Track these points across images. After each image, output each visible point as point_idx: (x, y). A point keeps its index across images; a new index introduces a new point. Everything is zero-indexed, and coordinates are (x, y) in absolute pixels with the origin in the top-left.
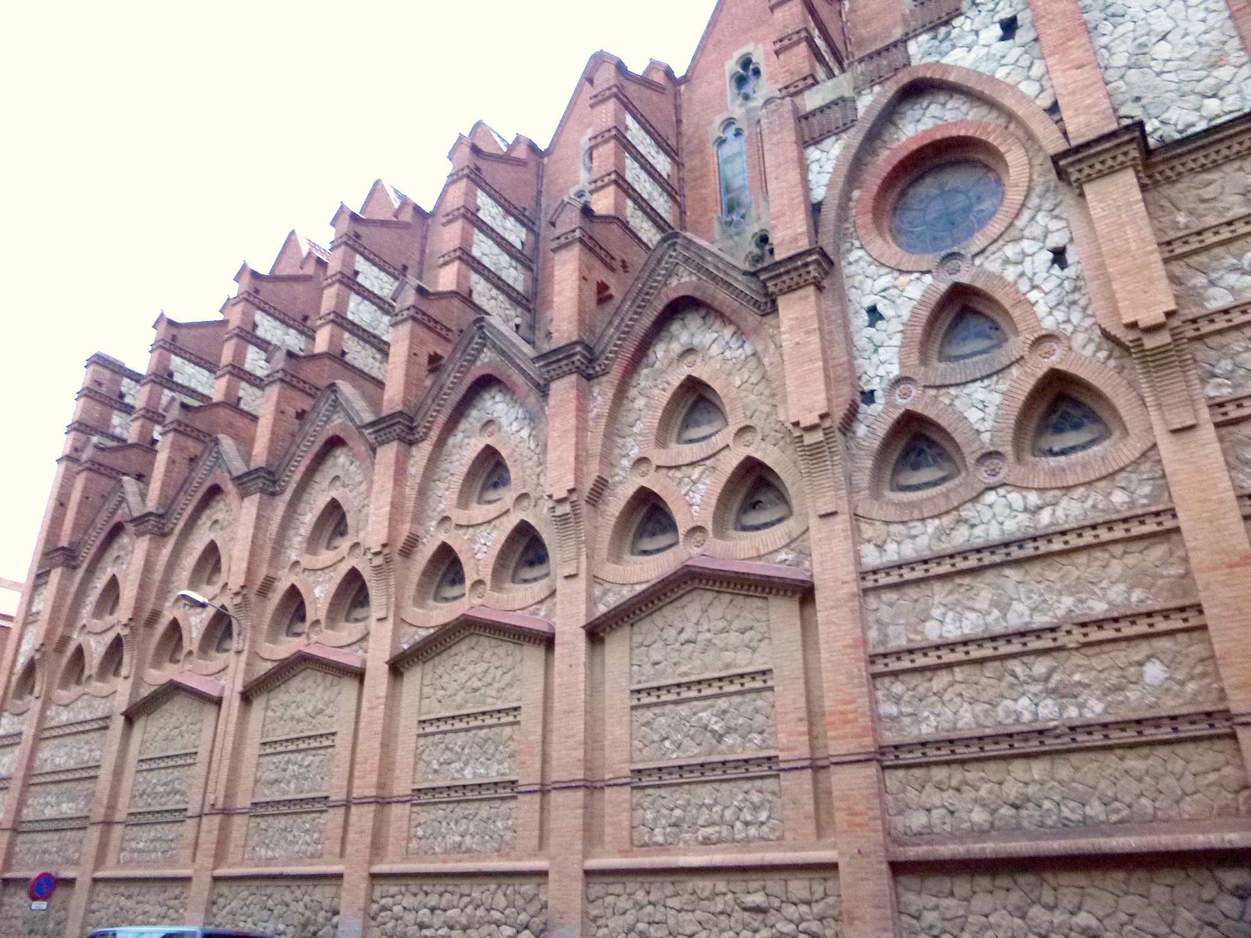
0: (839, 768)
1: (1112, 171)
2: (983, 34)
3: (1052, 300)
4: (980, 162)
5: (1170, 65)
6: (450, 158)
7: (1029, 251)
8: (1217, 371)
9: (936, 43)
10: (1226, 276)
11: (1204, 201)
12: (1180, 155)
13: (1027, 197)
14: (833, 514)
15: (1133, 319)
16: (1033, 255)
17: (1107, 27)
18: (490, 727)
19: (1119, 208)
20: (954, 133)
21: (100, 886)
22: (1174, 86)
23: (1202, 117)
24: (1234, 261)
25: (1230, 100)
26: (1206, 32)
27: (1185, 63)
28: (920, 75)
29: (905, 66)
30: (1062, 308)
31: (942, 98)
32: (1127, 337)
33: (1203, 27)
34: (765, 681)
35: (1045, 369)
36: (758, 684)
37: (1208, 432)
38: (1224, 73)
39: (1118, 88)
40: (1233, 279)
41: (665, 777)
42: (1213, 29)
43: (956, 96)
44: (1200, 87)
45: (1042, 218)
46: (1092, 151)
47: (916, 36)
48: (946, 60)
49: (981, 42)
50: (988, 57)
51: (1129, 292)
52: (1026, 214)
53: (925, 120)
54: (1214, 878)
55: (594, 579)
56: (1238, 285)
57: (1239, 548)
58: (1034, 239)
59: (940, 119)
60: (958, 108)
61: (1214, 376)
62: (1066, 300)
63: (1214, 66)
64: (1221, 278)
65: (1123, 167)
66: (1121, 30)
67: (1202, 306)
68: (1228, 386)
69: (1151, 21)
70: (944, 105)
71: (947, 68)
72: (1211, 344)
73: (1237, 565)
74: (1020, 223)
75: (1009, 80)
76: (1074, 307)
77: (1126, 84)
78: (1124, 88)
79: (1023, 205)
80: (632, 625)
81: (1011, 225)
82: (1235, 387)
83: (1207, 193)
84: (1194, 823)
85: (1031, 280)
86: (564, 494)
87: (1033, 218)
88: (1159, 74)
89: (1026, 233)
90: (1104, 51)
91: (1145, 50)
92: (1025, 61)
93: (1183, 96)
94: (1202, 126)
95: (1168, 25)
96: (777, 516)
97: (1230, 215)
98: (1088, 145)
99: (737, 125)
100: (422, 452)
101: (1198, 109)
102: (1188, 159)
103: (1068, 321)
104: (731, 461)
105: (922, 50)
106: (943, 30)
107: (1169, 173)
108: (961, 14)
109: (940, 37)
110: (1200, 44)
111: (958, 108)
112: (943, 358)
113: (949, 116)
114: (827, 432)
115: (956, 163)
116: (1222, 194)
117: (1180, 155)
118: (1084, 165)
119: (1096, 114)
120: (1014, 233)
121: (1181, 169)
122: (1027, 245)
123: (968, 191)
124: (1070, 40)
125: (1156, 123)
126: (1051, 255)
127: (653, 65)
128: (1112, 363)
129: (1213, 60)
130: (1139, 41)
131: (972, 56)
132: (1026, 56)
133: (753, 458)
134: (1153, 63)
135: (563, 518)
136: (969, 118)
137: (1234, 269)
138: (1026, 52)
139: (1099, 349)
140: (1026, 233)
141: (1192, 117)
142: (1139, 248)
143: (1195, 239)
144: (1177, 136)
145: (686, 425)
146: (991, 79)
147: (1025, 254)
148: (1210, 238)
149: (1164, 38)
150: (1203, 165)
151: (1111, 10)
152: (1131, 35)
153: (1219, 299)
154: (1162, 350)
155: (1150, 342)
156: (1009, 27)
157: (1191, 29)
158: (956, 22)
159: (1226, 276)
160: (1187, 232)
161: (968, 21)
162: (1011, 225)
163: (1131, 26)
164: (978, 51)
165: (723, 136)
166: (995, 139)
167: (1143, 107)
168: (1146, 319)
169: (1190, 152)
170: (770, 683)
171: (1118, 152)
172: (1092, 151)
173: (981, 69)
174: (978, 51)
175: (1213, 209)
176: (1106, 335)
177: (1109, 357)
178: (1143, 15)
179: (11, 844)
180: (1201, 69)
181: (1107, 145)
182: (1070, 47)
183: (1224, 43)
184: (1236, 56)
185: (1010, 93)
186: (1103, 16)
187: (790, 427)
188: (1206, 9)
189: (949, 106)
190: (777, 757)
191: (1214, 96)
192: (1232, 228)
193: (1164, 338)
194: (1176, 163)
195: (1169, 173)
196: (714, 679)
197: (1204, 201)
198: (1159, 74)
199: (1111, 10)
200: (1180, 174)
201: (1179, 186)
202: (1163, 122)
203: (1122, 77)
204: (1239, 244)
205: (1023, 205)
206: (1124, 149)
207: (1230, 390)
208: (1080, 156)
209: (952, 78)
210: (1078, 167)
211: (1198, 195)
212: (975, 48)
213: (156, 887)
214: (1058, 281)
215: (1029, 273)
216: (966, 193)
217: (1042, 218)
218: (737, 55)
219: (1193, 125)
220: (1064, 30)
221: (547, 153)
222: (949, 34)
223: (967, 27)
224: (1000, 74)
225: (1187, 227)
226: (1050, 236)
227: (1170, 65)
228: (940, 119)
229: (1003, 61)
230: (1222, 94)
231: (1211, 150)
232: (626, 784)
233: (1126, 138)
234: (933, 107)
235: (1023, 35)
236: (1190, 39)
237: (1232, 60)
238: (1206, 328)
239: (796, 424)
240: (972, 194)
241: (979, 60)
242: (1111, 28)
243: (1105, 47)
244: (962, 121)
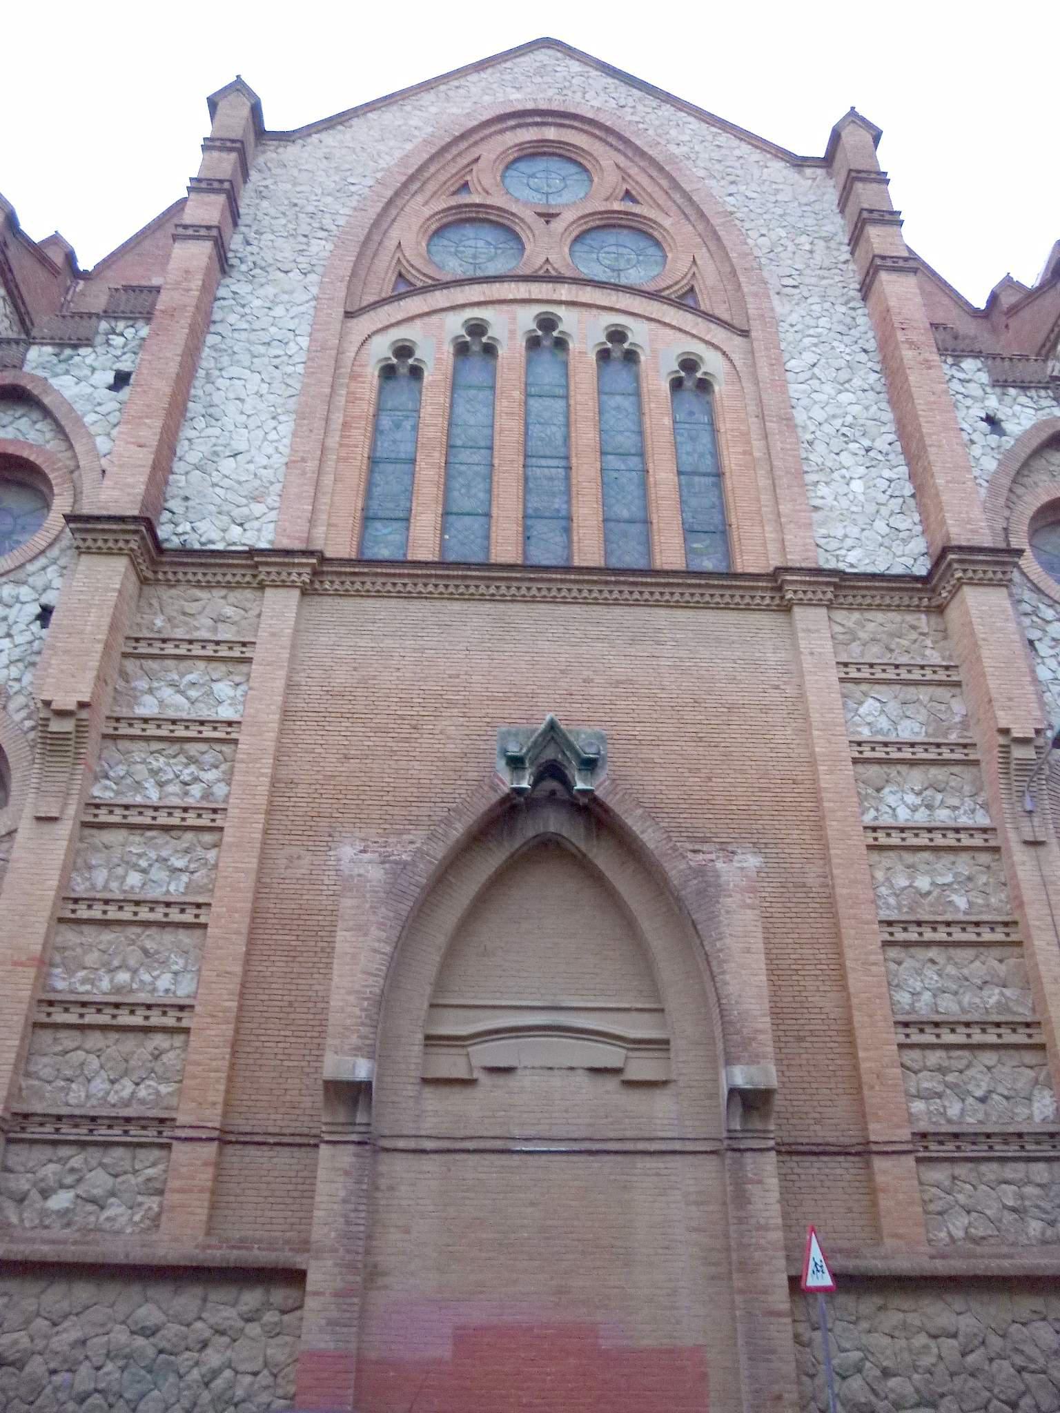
1: (110, 553)
2: (97, 375)
3: (17, 653)
4: (41, 492)
5: (226, 483)
7: (23, 599)
8: (112, 774)
9: (55, 359)
10: (164, 689)
11: (184, 614)
12: (186, 564)
13: (51, 545)
14: (54, 819)
15: (1006, 726)
16: (23, 603)
17: (200, 423)
18: (948, 1047)
19: (97, 589)
20: (25, 454)
22: (218, 501)
23: (223, 539)
24: (176, 677)
25: (249, 534)
26: (265, 468)
27: (236, 486)
28: (23, 382)
29: (15, 367)
30: (20, 665)
31: (35, 415)
33: (265, 461)
37: (65, 829)
38: (258, 509)
39: (178, 481)
40: (167, 693)
41: (65, 1129)
42: (271, 467)
43: (49, 421)
44: (236, 512)
45: (52, 572)
46: (100, 526)
47: (42, 344)
48: (54, 382)
49: (92, 381)
50: (89, 398)
51: (62, 671)
52: (42, 561)
53: (10, 429)
56: (168, 701)
57: (32, 947)
58: (33, 588)
59: (24, 435)
60: (43, 432)
61: (107, 777)
62: (29, 658)
63: (256, 499)
64: (158, 689)
66: (210, 431)
67: (132, 708)
68: (113, 790)
69: (234, 436)
70: (35, 423)
71: (48, 388)
72: (120, 747)
73: (22, 964)
74: (30, 568)
75: (93, 430)
76: (31, 669)
77: (187, 481)
78: (182, 484)
79: (43, 552)
81: (22, 566)
82: (117, 793)
83: (192, 608)
85: (10, 627)
87: (44, 569)
88: (214, 485)
89: (31, 580)
90: (186, 442)
91: (215, 459)
92: (113, 419)
93: (219, 513)
94: (220, 546)
95: (242, 446)
97: (197, 635)
98: (98, 519)
101: (224, 531)
102: (190, 570)
103: (18, 680)
105: (41, 360)
106: (68, 352)
107: (170, 576)
108: (91, 346)
109: (62, 357)
110: (255, 475)
111: (43, 432)
113: (32, 436)
115: (21, 485)
116: (199, 613)
117: (186, 564)
118: (89, 536)
119: (129, 494)
120: (20, 575)
121: (180, 576)
122: (25, 592)
123: (19, 517)
124: (147, 417)
125: (188, 527)
126: (39, 610)
127: (55, 240)
128: (32, 735)
129: (256, 493)
130: (216, 448)
131: (76, 390)
132: (117, 413)
134: (215, 473)
136: (48, 447)
137: (173, 685)
138: (120, 410)
139: (29, 718)
140: (31, 580)
141: (215, 535)
142: (92, 633)
143: (158, 644)
144: (197, 546)
146: (78, 420)
147: (17, 600)
148: (170, 649)
149: (235, 455)
150: (199, 581)
151: (211, 410)
152: (213, 440)
153: (148, 707)
154: (63, 737)
156: (122, 380)
157: (257, 459)
158: (82, 351)
159: (164, 689)
160: (156, 636)
161: (93, 356)
162: (22, 566)
163: (217, 431)
164: (84, 389)
166: (56, 478)
167: (187, 508)
169: (193, 564)
171: (121, 537)
172: (100, 526)
173: (76, 406)
174: (84, 389)
175: (186, 624)
177: (33, 728)
178: (232, 428)
180: (245, 497)
181: (114, 527)
182: (145, 424)
183: (272, 483)
184: (273, 500)
185: (84, 441)
186: (203, 412)
187: (40, 705)
188: (276, 448)
189: (38, 426)
190: (174, 1120)
191: (241, 525)
192: (191, 647)
193: (67, 726)
194: (180, 570)
195: (170, 576)
196: (107, 1004)
197: (184, 614)
198: (214, 485)
199: (211, 410)
200: (178, 581)
201: (173, 592)
202: (193, 528)
203: (187, 473)
204: (189, 663)
205: (43, 552)
206: (127, 537)
207: (112, 795)
208: (89, 526)
209: (46, 400)
210: (84, 536)
211: (182, 606)
212: (83, 383)
214: (30, 638)
215: (11, 620)
216: (15, 518)
217: (52, 572)
219: (213, 542)
220: (148, 406)
222: (71, 357)
223: (88, 361)
224: (89, 419)
225: (159, 632)
226: (49, 592)
227: (226, 483)
228: (24, 435)
229: (98, 409)
230: (246, 526)
231: (210, 571)
233: (132, 527)
234: (24, 420)
235: (125, 393)
236: (251, 467)
237: (269, 501)
238: (124, 730)
239: (47, 704)
240: (19, 521)
241: (80, 396)
242: (203, 425)
243: (189, 440)
244: (40, 446)
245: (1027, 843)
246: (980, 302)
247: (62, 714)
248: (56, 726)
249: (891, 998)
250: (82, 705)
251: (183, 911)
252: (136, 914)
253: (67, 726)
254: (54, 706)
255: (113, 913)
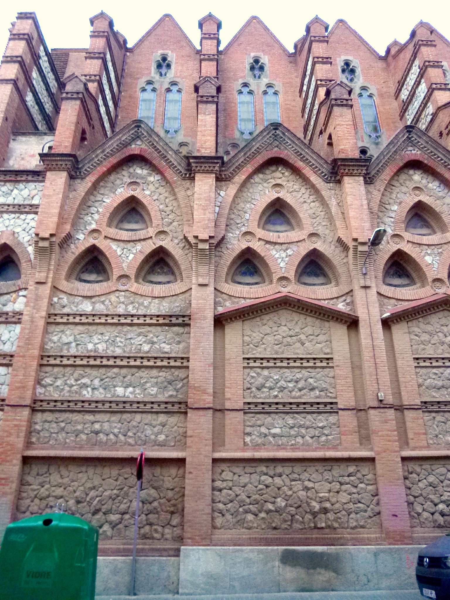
0: (229, 412)
6: (92, 22)
12: (349, 166)
14: (206, 285)
21: (35, 469)
32: (193, 241)
34: (328, 363)
35: (312, 248)
36: (324, 364)
54: (59, 472)
55: (55, 288)
65: (211, 172)
80: (243, 321)
84: (162, 445)
86: (47, 235)
96: (167, 280)
99: (180, 86)
100: (230, 190)
104: (149, 247)
112: (264, 228)
114: (51, 244)
117: (349, 166)
133: (319, 251)
135: (43, 249)
145: (121, 221)
155: (201, 246)
165: (146, 88)
168: (202, 236)
170: (331, 365)
176: (185, 238)
179: (31, 423)
193: (46, 244)
213: (319, 467)
218: (160, 52)
221: (130, 50)
232: (420, 409)
245: (362, 287)
246: (383, 53)
247: (43, 239)
248: (41, 244)
249: (96, 422)
250: (52, 235)
251: (55, 359)
252: (61, 361)
253: (46, 244)
254: (40, 236)
255: (105, 362)
